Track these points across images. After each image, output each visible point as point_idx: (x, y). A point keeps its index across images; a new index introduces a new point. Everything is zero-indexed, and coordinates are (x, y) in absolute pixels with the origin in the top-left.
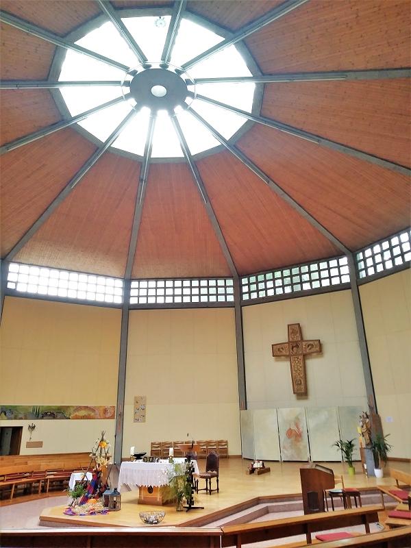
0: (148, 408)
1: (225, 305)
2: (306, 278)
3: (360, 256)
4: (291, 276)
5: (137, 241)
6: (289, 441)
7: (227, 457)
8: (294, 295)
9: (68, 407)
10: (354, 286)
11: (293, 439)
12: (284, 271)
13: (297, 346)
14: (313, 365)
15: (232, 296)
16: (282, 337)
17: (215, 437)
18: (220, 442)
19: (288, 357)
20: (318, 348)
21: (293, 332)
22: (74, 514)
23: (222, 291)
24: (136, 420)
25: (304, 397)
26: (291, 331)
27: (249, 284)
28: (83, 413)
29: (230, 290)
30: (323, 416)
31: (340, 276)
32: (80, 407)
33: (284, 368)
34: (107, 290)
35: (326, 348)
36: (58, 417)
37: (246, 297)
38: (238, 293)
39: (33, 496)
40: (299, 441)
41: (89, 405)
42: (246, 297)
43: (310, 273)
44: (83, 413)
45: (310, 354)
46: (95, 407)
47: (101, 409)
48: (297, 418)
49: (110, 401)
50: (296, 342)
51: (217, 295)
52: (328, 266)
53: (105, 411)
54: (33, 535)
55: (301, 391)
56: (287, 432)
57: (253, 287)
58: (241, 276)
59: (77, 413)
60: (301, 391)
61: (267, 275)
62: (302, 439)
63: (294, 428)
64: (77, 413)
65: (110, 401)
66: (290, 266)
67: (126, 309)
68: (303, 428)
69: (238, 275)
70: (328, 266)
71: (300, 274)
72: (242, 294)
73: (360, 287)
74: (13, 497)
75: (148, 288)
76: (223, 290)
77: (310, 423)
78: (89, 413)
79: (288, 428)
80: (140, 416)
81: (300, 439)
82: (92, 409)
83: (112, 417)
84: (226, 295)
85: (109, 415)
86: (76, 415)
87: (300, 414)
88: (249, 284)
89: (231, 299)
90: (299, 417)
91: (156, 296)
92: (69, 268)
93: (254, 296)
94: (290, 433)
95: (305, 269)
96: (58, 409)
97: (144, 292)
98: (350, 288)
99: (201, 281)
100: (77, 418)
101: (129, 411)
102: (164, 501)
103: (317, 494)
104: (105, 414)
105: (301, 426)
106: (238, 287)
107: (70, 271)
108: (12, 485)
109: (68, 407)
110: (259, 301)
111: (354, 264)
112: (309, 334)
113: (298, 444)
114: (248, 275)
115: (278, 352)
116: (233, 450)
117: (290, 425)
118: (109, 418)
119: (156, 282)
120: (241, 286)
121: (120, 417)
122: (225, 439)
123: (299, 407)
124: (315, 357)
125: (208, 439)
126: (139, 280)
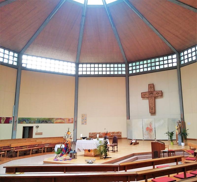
0: (87, 119)
1: (122, 75)
3: (182, 54)
8: (152, 71)
9: (53, 118)
10: (127, 76)
11: (149, 131)
13: (152, 93)
14: (159, 101)
16: (146, 89)
17: (116, 131)
18: (118, 133)
20: (161, 94)
21: (150, 88)
24: (83, 124)
28: (59, 121)
29: (124, 69)
31: (192, 57)
32: (58, 118)
33: (146, 103)
35: (165, 95)
36: (49, 122)
37: (130, 72)
38: (127, 70)
41: (62, 118)
42: (130, 72)
44: (59, 121)
45: (157, 97)
47: (67, 119)
48: (151, 123)
49: (71, 116)
50: (152, 92)
53: (69, 120)
55: (153, 112)
57: (134, 68)
58: (129, 63)
60: (153, 112)
63: (149, 127)
65: (71, 116)
67: (77, 77)
68: (153, 127)
69: (128, 62)
72: (129, 71)
75: (87, 68)
76: (121, 69)
78: (62, 121)
79: (147, 127)
80: (84, 122)
82: (63, 119)
83: (72, 123)
84: (122, 71)
85: (71, 122)
88: (132, 66)
93: (134, 72)
94: (147, 129)
97: (84, 69)
99: (118, 65)
100: (57, 123)
104: (69, 121)
105: (152, 126)
106: (127, 68)
110: (137, 74)
112: (157, 88)
113: (151, 133)
114: (132, 62)
115: (143, 96)
117: (148, 126)
118: (71, 123)
119: (91, 65)
120: (129, 67)
122: (120, 131)
124: (160, 98)
126: (83, 64)
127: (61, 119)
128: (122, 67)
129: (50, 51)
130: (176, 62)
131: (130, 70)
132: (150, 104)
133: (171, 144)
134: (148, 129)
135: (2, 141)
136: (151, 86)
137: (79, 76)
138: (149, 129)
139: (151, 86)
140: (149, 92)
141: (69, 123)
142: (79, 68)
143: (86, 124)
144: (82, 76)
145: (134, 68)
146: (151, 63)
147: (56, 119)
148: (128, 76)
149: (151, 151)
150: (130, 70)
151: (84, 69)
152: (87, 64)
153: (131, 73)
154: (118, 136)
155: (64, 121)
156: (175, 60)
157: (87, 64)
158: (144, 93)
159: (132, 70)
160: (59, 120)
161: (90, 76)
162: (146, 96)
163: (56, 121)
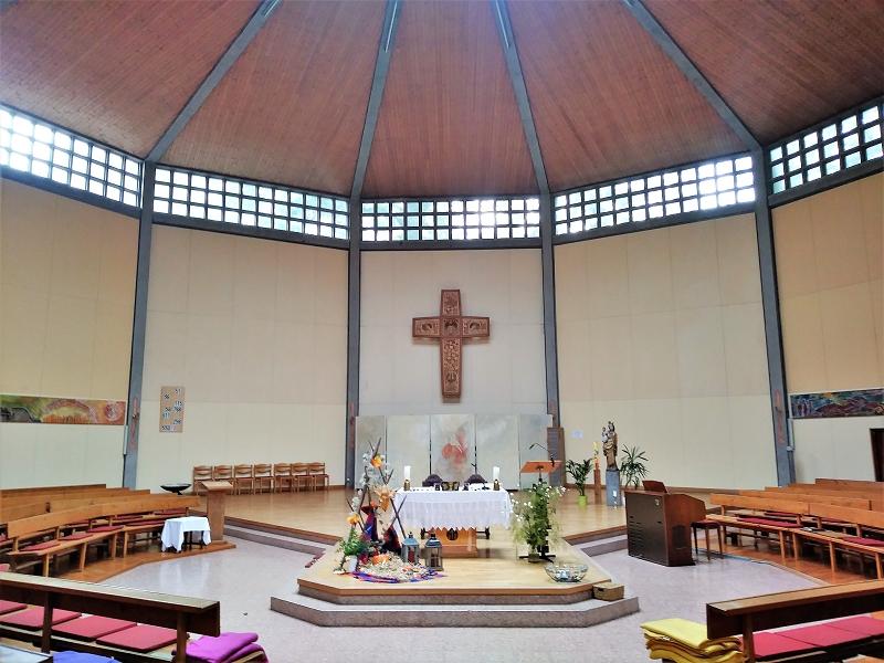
0: (188, 409)
2: (428, 221)
4: (406, 215)
5: (214, 90)
6: (446, 462)
7: (322, 489)
8: (405, 246)
9: (37, 399)
10: (547, 243)
11: (453, 458)
12: (683, 172)
13: (455, 325)
14: (474, 355)
15: (344, 231)
16: (430, 307)
17: (306, 460)
18: (313, 467)
19: (437, 339)
20: (482, 330)
22: (367, 577)
23: (399, 221)
24: (164, 428)
25: (455, 399)
26: (446, 300)
27: (376, 215)
28: (65, 412)
30: (501, 426)
32: (60, 400)
33: (429, 355)
34: (119, 180)
35: (495, 331)
36: (17, 417)
38: (355, 227)
39: (113, 563)
40: (460, 462)
41: (77, 398)
43: (435, 214)
44: (65, 412)
45: (470, 338)
46: (88, 401)
47: (100, 406)
48: (461, 429)
49: (117, 394)
50: (454, 318)
51: (435, 228)
52: (583, 198)
53: (107, 410)
54: (772, 607)
56: (445, 448)
58: (553, 193)
59: (55, 412)
61: (571, 196)
62: (466, 460)
63: (455, 443)
64: (55, 412)
65: (117, 394)
66: (407, 197)
68: (469, 443)
70: (583, 198)
71: (420, 214)
72: (554, 224)
73: (556, 247)
74: (85, 566)
76: (327, 219)
77: (478, 437)
78: (77, 413)
80: (172, 419)
81: (463, 459)
82: (84, 406)
83: (118, 422)
84: (334, 226)
85: (114, 418)
86: (52, 416)
87: (466, 423)
88: (376, 215)
89: (342, 234)
90: (465, 428)
91: (664, 203)
92: (38, 112)
94: (448, 451)
95: (428, 207)
96: (16, 403)
97: (178, 193)
98: (541, 247)
100: (53, 421)
101: (150, 411)
102: (526, 550)
103: (683, 527)
104: (106, 415)
105: (465, 440)
107: (37, 118)
108: (82, 545)
109: (36, 399)
110: (390, 246)
111: (548, 212)
112: (472, 307)
113: (460, 466)
114: (376, 199)
115: (421, 330)
116: (336, 477)
117: (449, 439)
118: (114, 423)
119: (225, 181)
120: (553, 209)
121: (130, 418)
122: (321, 462)
123: (448, 419)
124: (475, 343)
125: (238, 464)
126: (173, 168)
127: (72, 402)
128: (334, 212)
129: (41, 74)
130: (365, 229)
131: (560, 223)
132: (445, 362)
133: (577, 503)
134: (450, 450)
135: (6, 493)
136: (451, 298)
137: (156, 220)
138: (453, 449)
139: (451, 298)
140: (441, 317)
141: (108, 423)
142: (558, 227)
143: (181, 431)
144: (169, 220)
145: (575, 212)
146: (583, 204)
147: (50, 402)
148: (547, 242)
149: (625, 523)
150: (560, 223)
151: (178, 193)
152: (73, 138)
153: (611, 224)
154: (243, 484)
155: (84, 415)
156: (535, 218)
157: (734, 160)
158: (424, 322)
159: (569, 221)
160: (65, 409)
161: (204, 225)
162: (432, 332)
163: (51, 413)
